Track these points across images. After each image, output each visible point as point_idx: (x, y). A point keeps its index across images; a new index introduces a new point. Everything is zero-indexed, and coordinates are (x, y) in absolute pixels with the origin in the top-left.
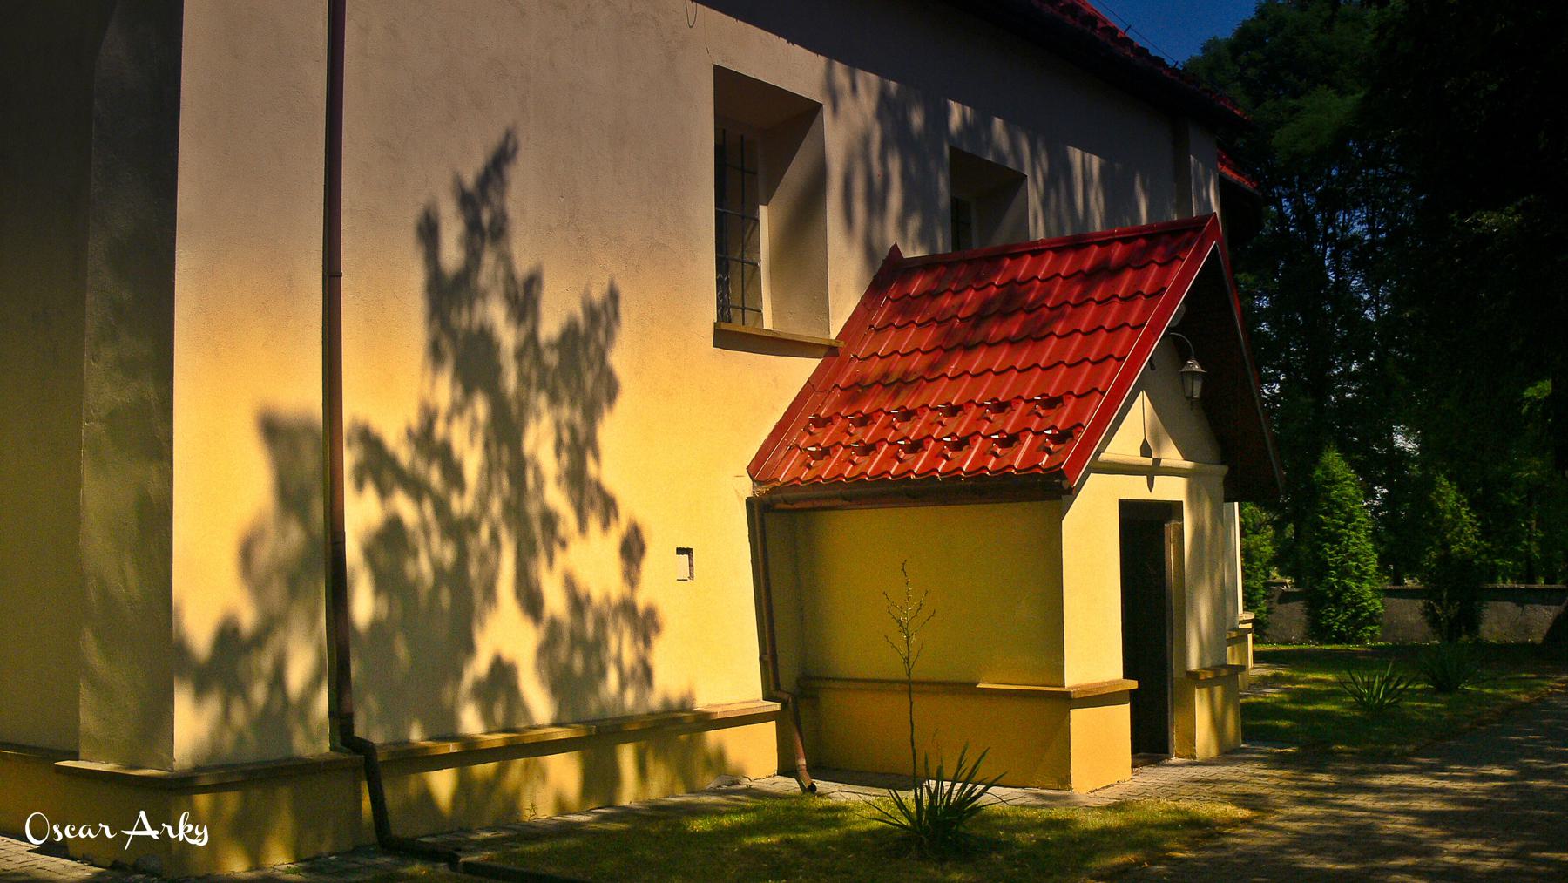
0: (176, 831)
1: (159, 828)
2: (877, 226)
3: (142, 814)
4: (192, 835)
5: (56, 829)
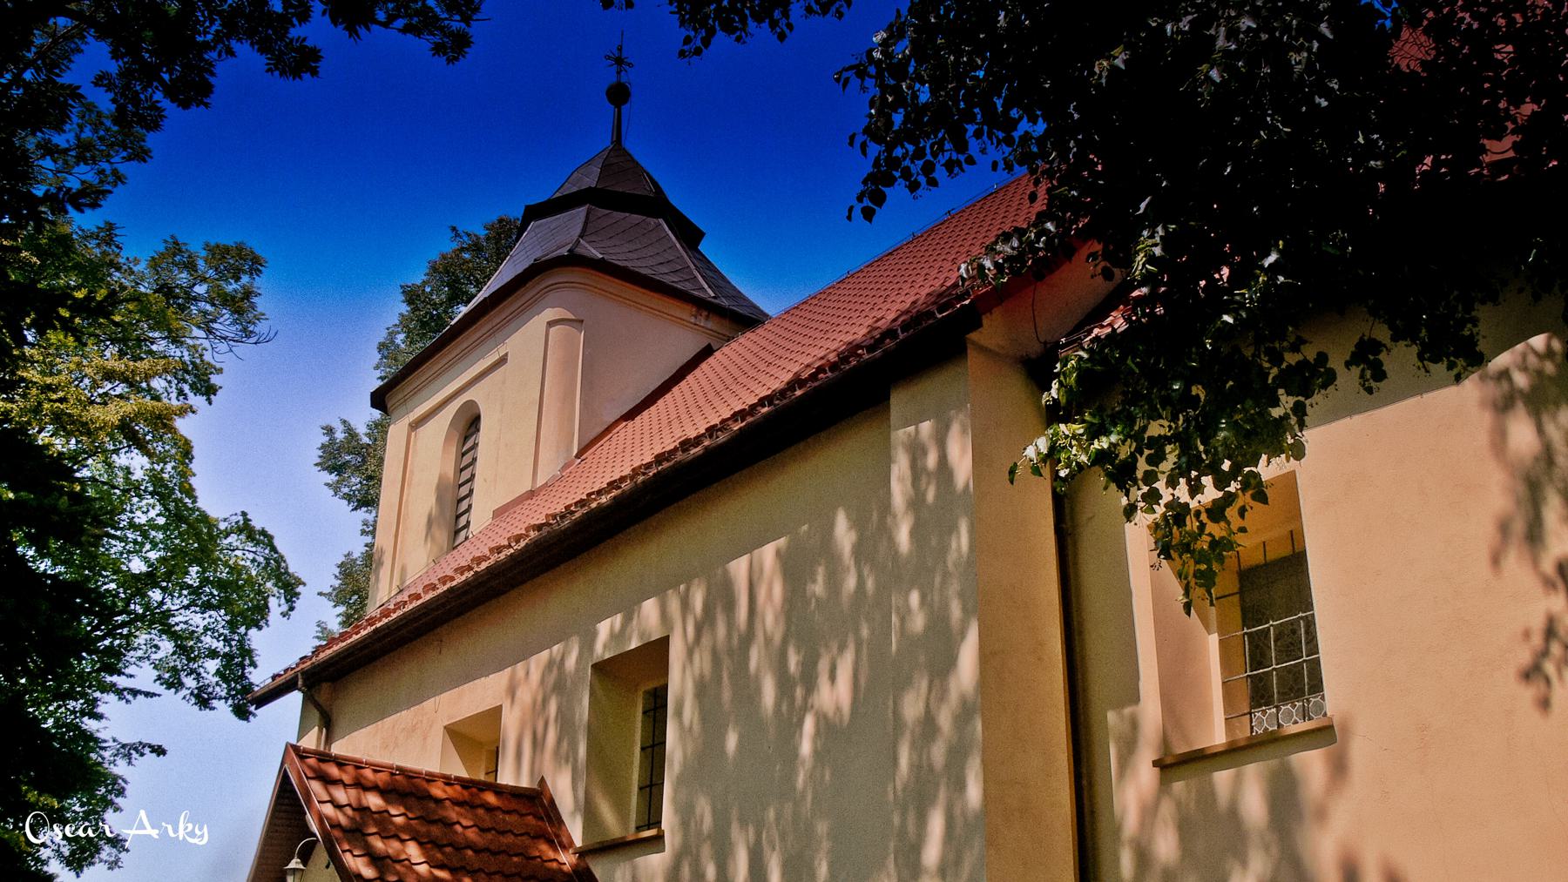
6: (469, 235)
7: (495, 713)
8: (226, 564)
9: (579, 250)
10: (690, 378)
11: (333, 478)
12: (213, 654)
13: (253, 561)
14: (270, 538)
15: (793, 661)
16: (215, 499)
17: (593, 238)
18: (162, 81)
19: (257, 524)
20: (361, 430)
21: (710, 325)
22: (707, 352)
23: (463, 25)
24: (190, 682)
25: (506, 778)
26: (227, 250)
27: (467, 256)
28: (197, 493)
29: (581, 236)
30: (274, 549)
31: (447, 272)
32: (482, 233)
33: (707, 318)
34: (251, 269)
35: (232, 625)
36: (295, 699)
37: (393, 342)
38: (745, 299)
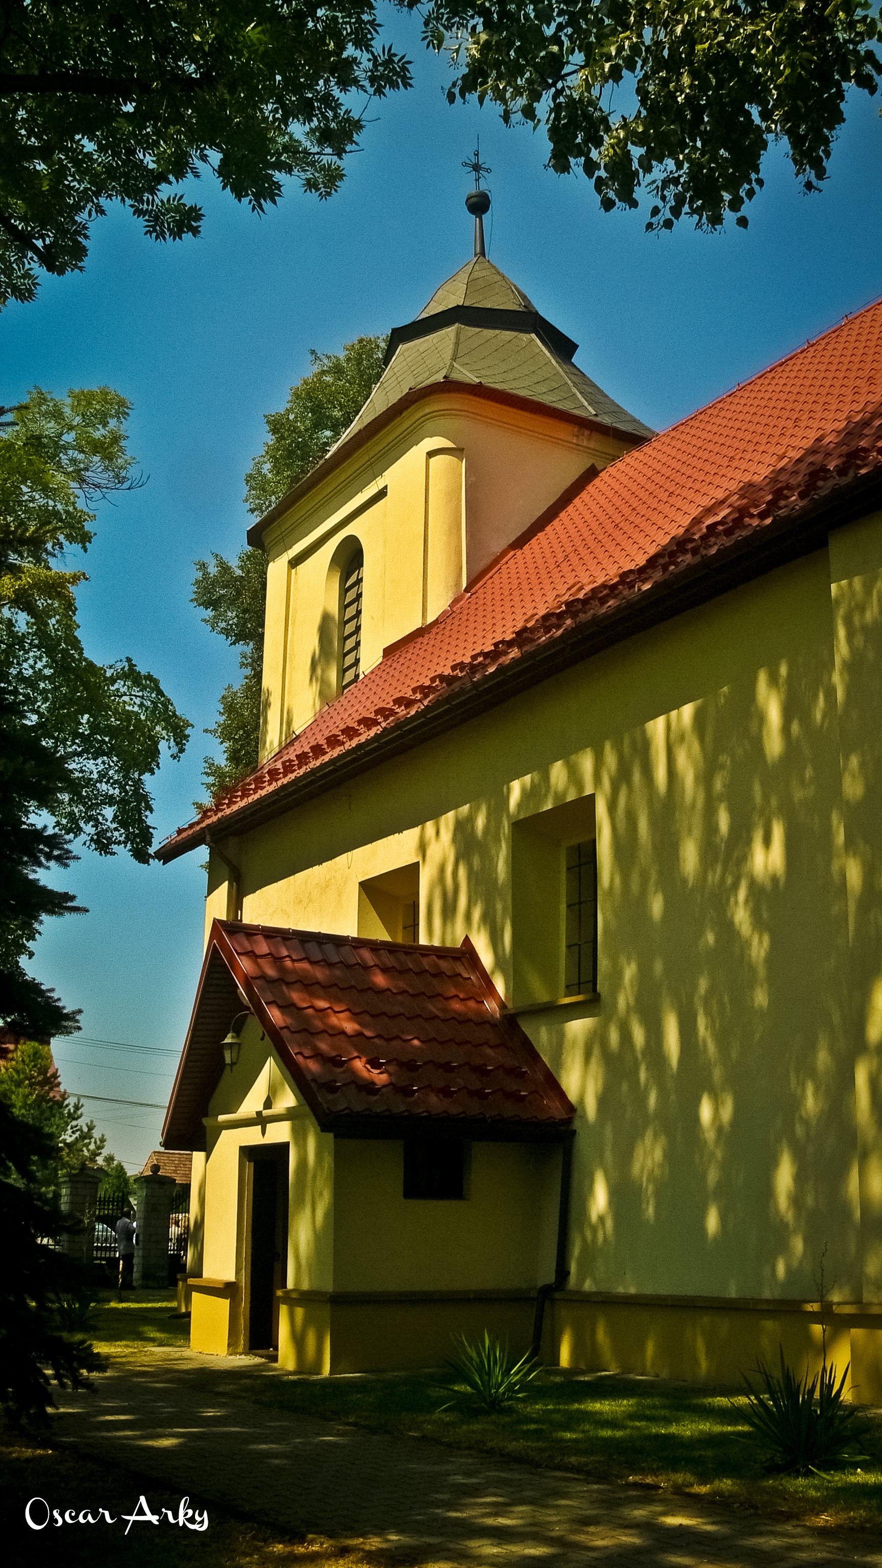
0: (176, 1516)
1: (159, 1513)
2: (449, 930)
3: (142, 1499)
4: (192, 1520)
5: (56, 1513)
6: (329, 357)
7: (412, 871)
8: (116, 712)
9: (455, 376)
10: (577, 501)
11: (209, 613)
12: (110, 800)
13: (141, 705)
14: (156, 682)
15: (724, 821)
16: (99, 650)
17: (466, 360)
18: (35, 249)
19: (142, 669)
20: (234, 563)
21: (592, 445)
22: (591, 474)
23: (335, 158)
24: (89, 829)
25: (423, 940)
26: (92, 395)
27: (328, 379)
28: (84, 645)
29: (454, 358)
30: (160, 693)
31: (310, 399)
32: (342, 355)
33: (589, 438)
34: (117, 412)
35: (125, 770)
36: (202, 853)
37: (259, 473)
38: (625, 413)
